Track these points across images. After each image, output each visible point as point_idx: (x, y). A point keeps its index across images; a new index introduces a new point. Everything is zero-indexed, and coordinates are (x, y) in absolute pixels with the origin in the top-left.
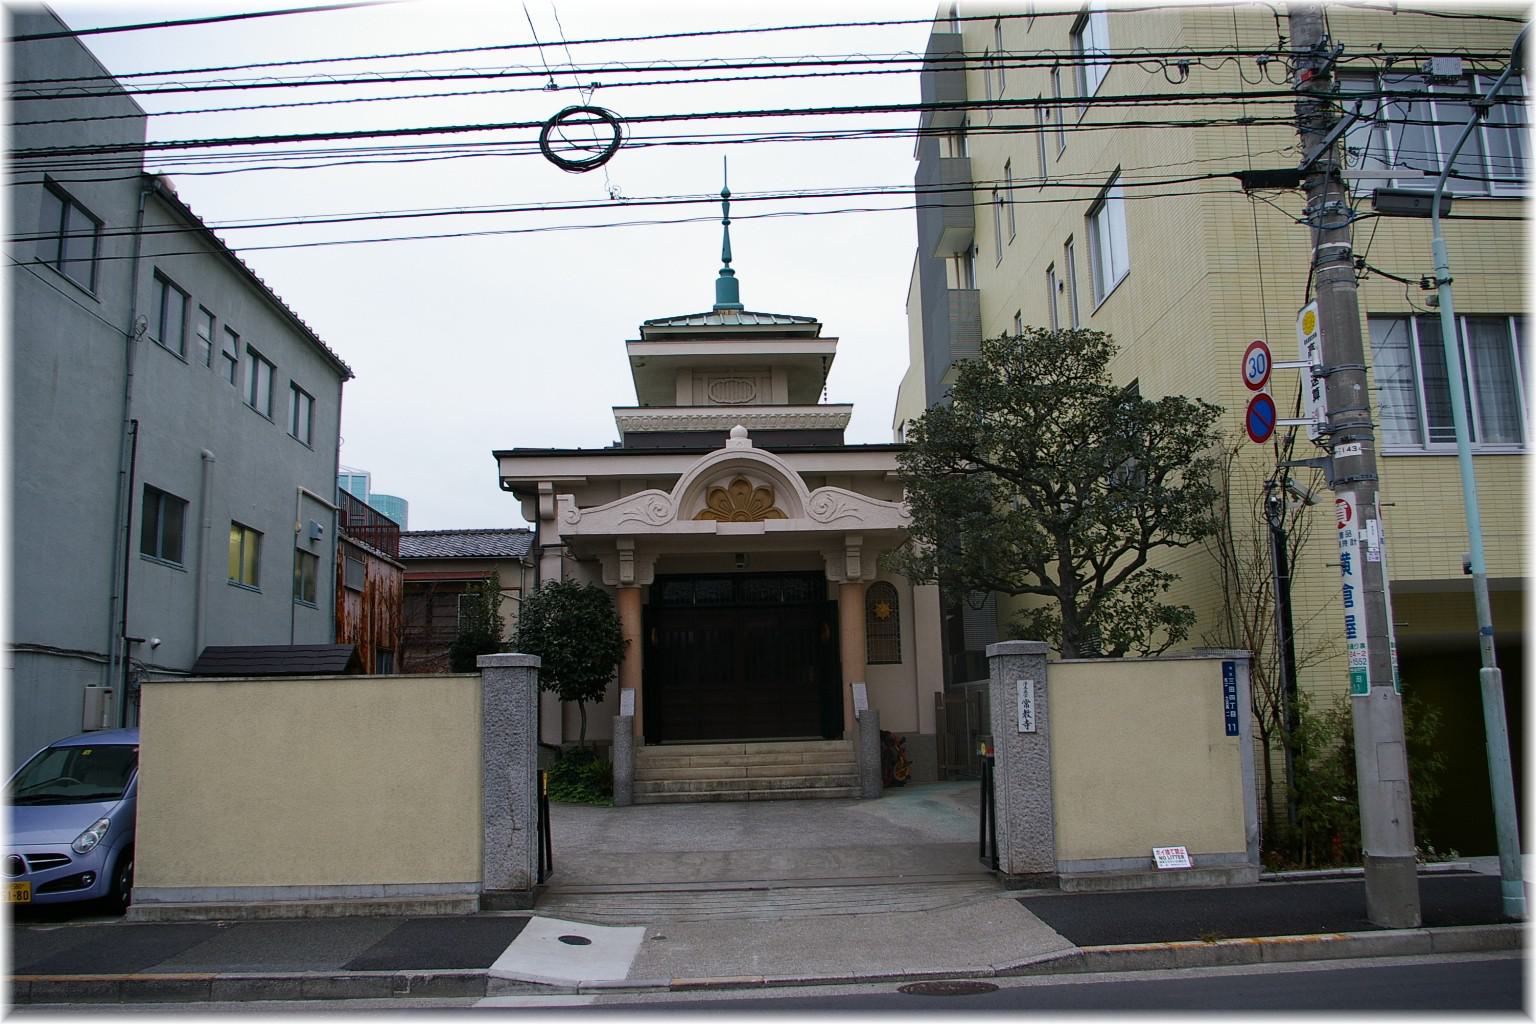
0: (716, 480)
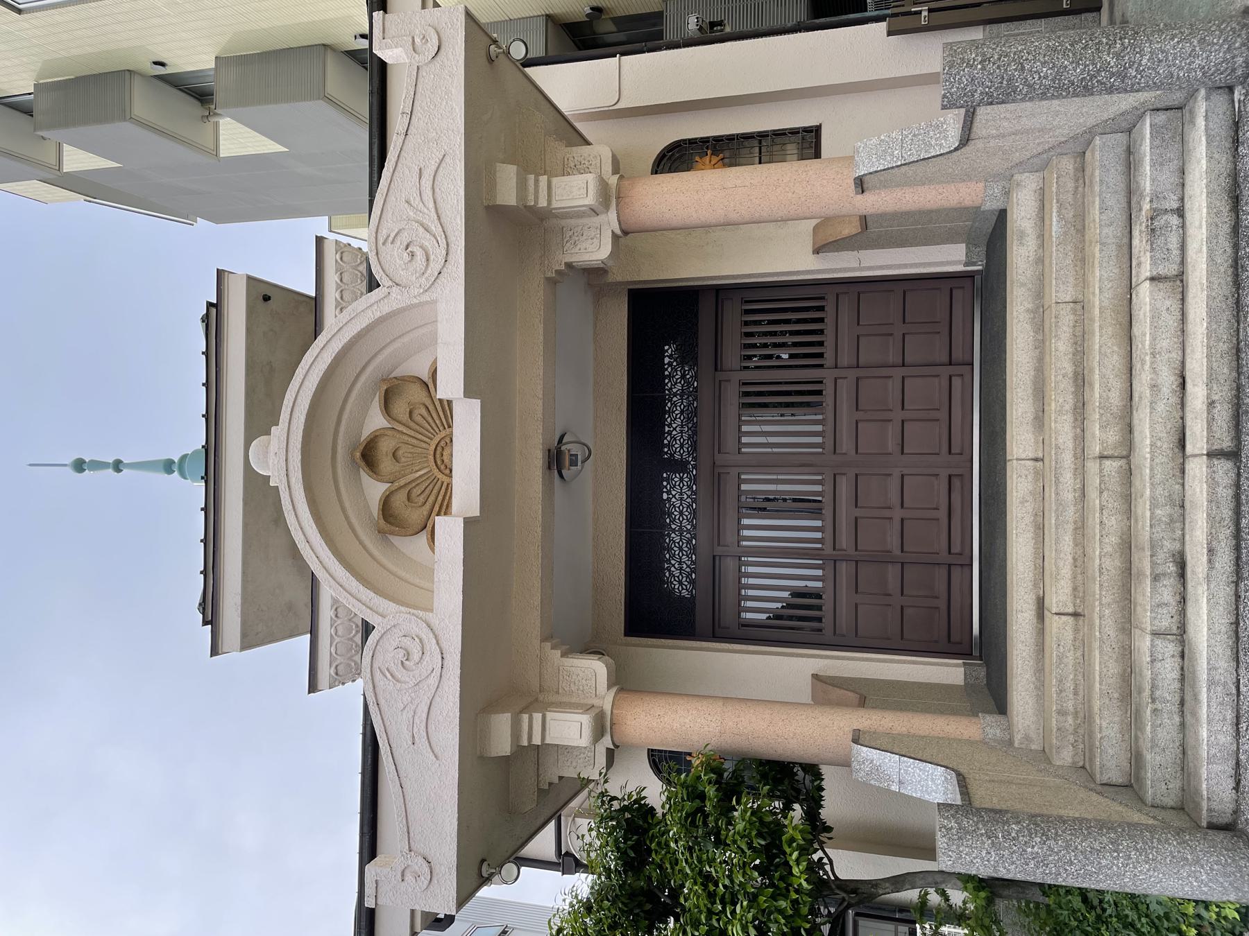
0: (367, 507)
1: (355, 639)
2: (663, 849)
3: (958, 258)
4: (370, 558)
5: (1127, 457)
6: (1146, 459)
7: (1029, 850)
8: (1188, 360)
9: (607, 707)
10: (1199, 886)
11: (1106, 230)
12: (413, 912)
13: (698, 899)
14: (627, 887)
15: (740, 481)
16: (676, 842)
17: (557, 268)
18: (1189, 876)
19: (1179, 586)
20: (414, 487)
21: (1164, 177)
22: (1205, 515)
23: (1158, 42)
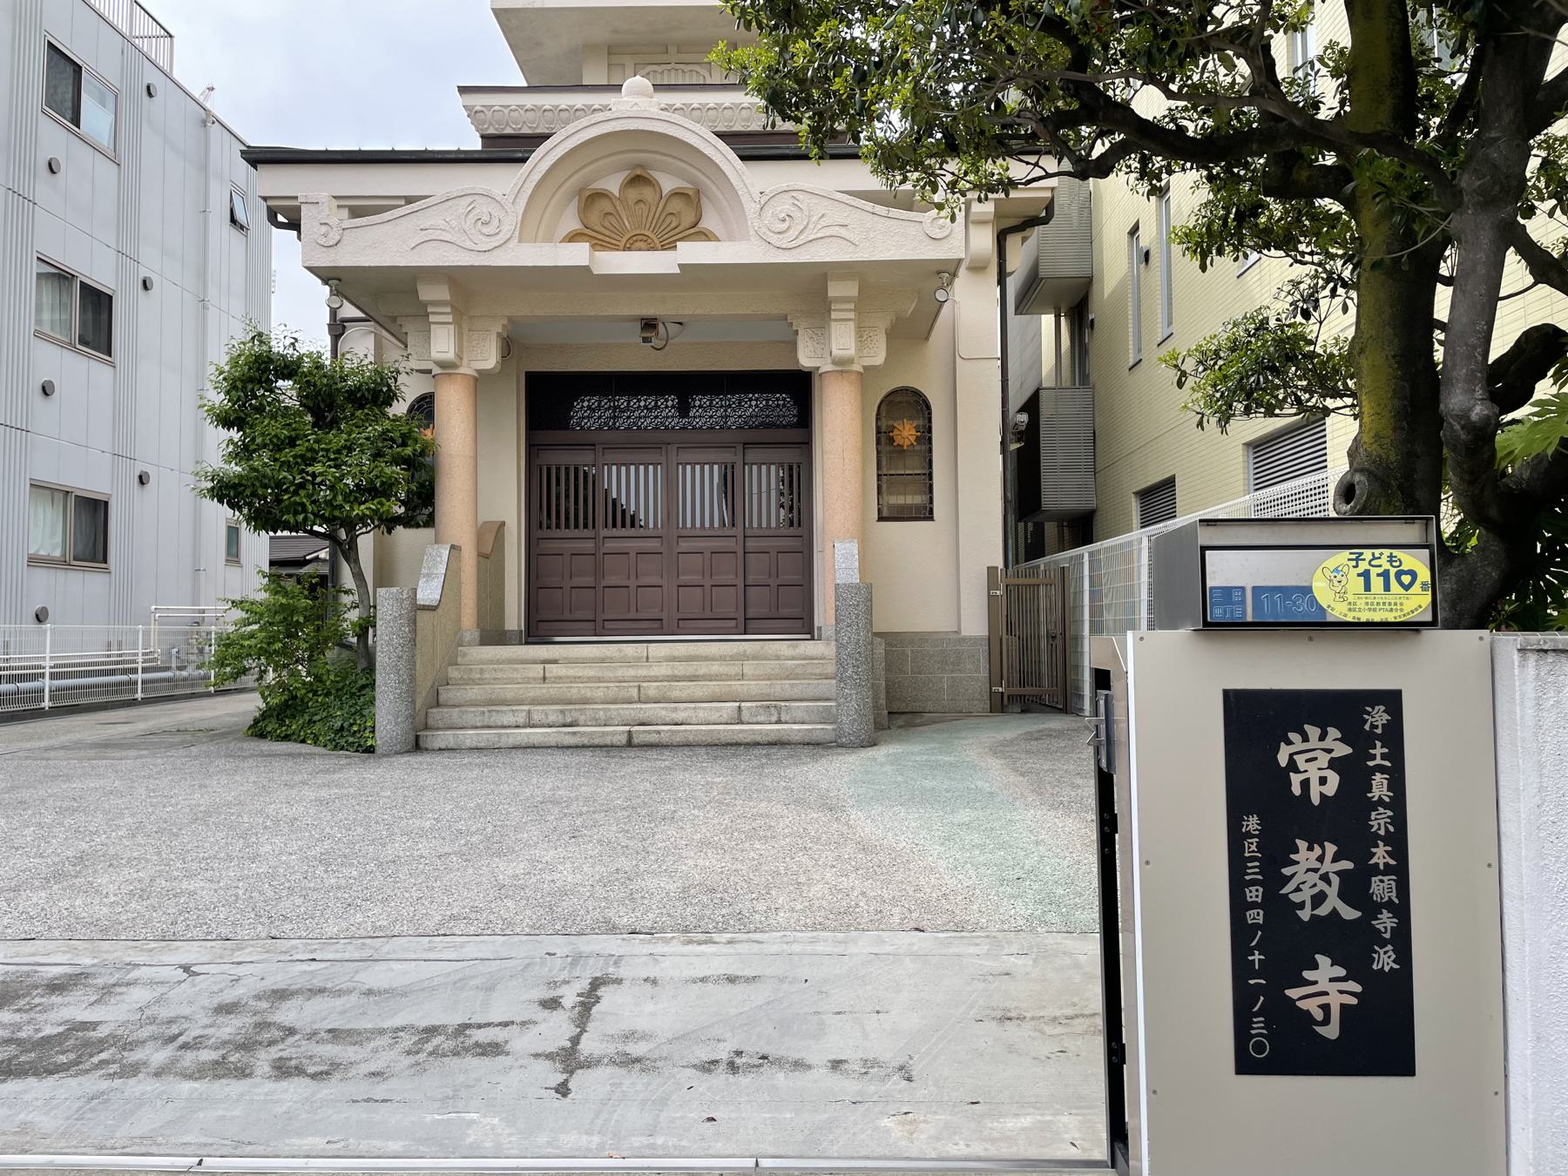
9: (461, 370)
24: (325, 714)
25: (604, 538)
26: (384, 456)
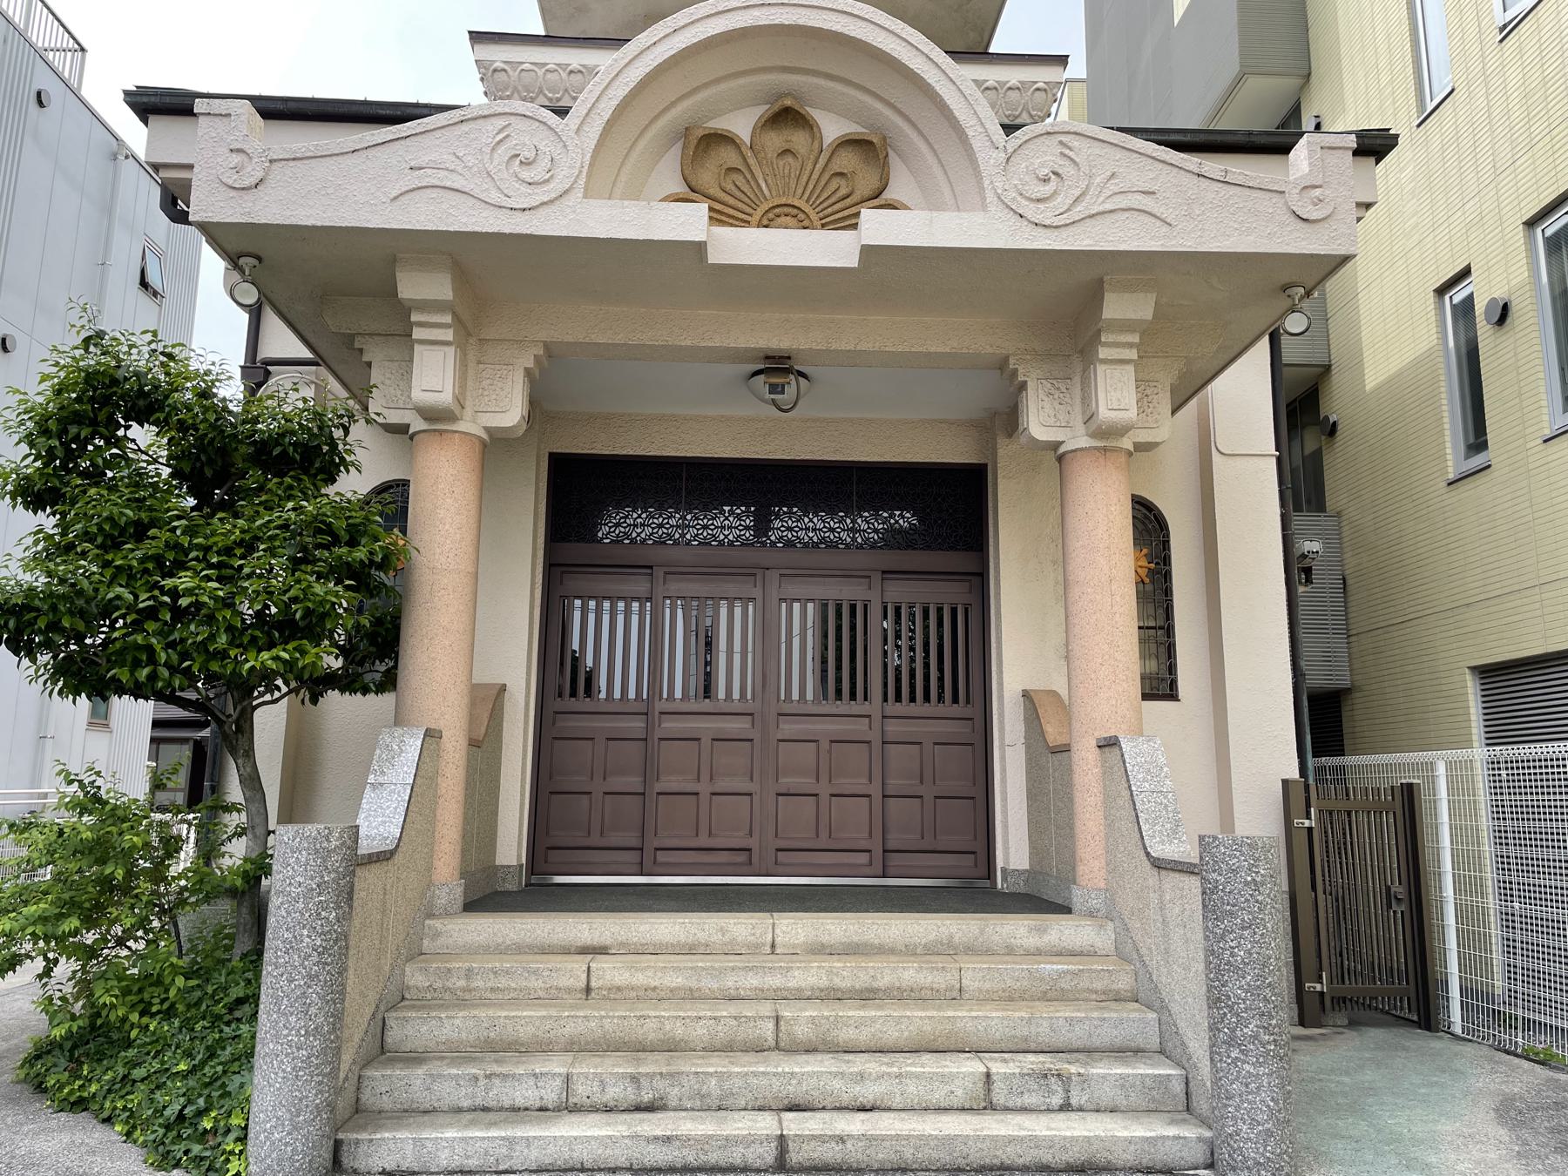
1: (541, 96)
2: (285, 492)
3: (1012, 860)
4: (652, 115)
5: (777, 1048)
6: (776, 1067)
7: (305, 932)
8: (892, 1115)
9: (462, 426)
10: (265, 1131)
11: (1045, 1024)
12: (190, 167)
13: (222, 534)
14: (234, 445)
15: (731, 601)
16: (294, 509)
17: (1021, 371)
18: (278, 1118)
19: (625, 1105)
20: (745, 177)
21: (1108, 1089)
22: (710, 1133)
23: (1270, 1083)
24: (156, 1066)
25: (661, 713)
26: (314, 561)
